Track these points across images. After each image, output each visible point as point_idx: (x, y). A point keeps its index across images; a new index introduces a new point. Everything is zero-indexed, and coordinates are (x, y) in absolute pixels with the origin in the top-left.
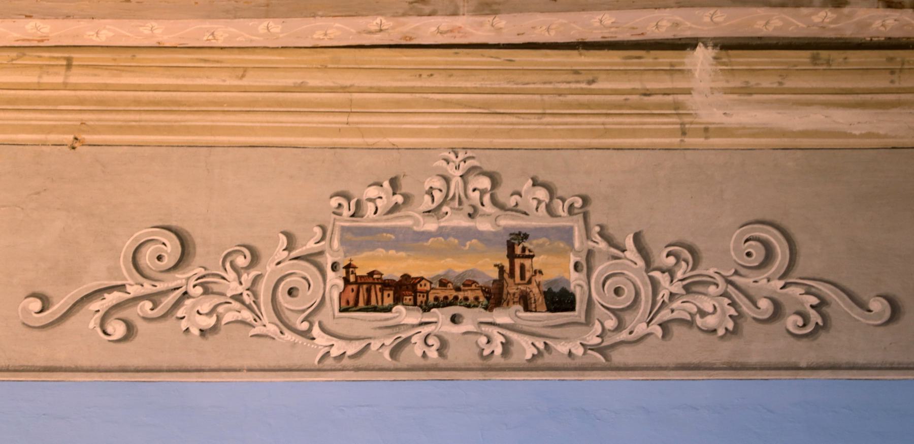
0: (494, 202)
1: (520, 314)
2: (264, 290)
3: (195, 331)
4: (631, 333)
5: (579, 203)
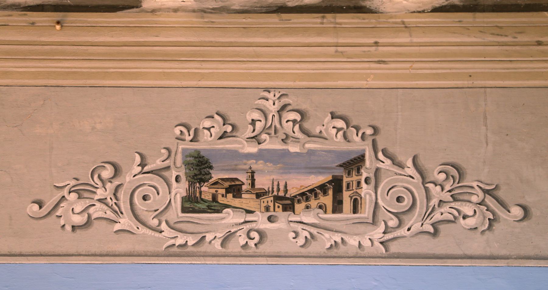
0: (302, 129)
1: (320, 215)
2: (123, 196)
3: (68, 228)
4: (409, 229)
5: (369, 131)
